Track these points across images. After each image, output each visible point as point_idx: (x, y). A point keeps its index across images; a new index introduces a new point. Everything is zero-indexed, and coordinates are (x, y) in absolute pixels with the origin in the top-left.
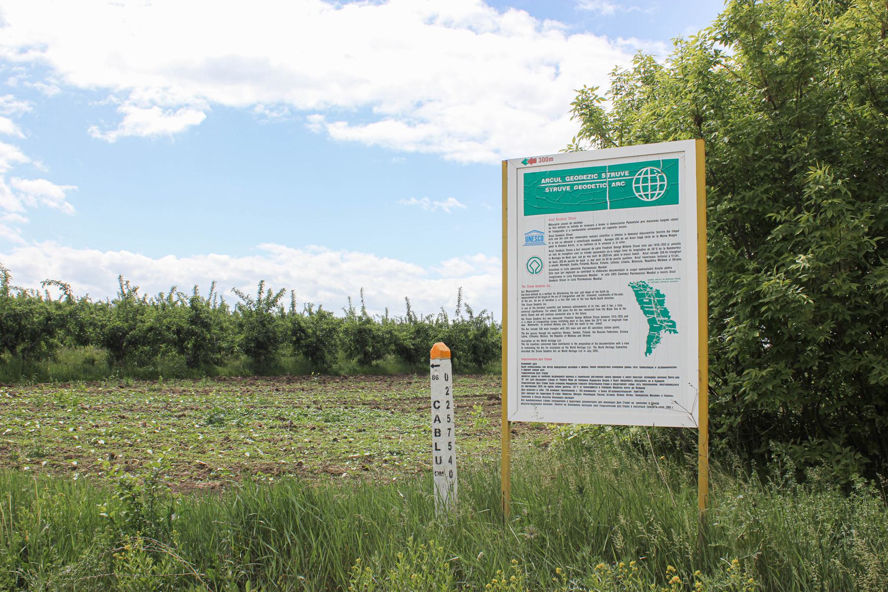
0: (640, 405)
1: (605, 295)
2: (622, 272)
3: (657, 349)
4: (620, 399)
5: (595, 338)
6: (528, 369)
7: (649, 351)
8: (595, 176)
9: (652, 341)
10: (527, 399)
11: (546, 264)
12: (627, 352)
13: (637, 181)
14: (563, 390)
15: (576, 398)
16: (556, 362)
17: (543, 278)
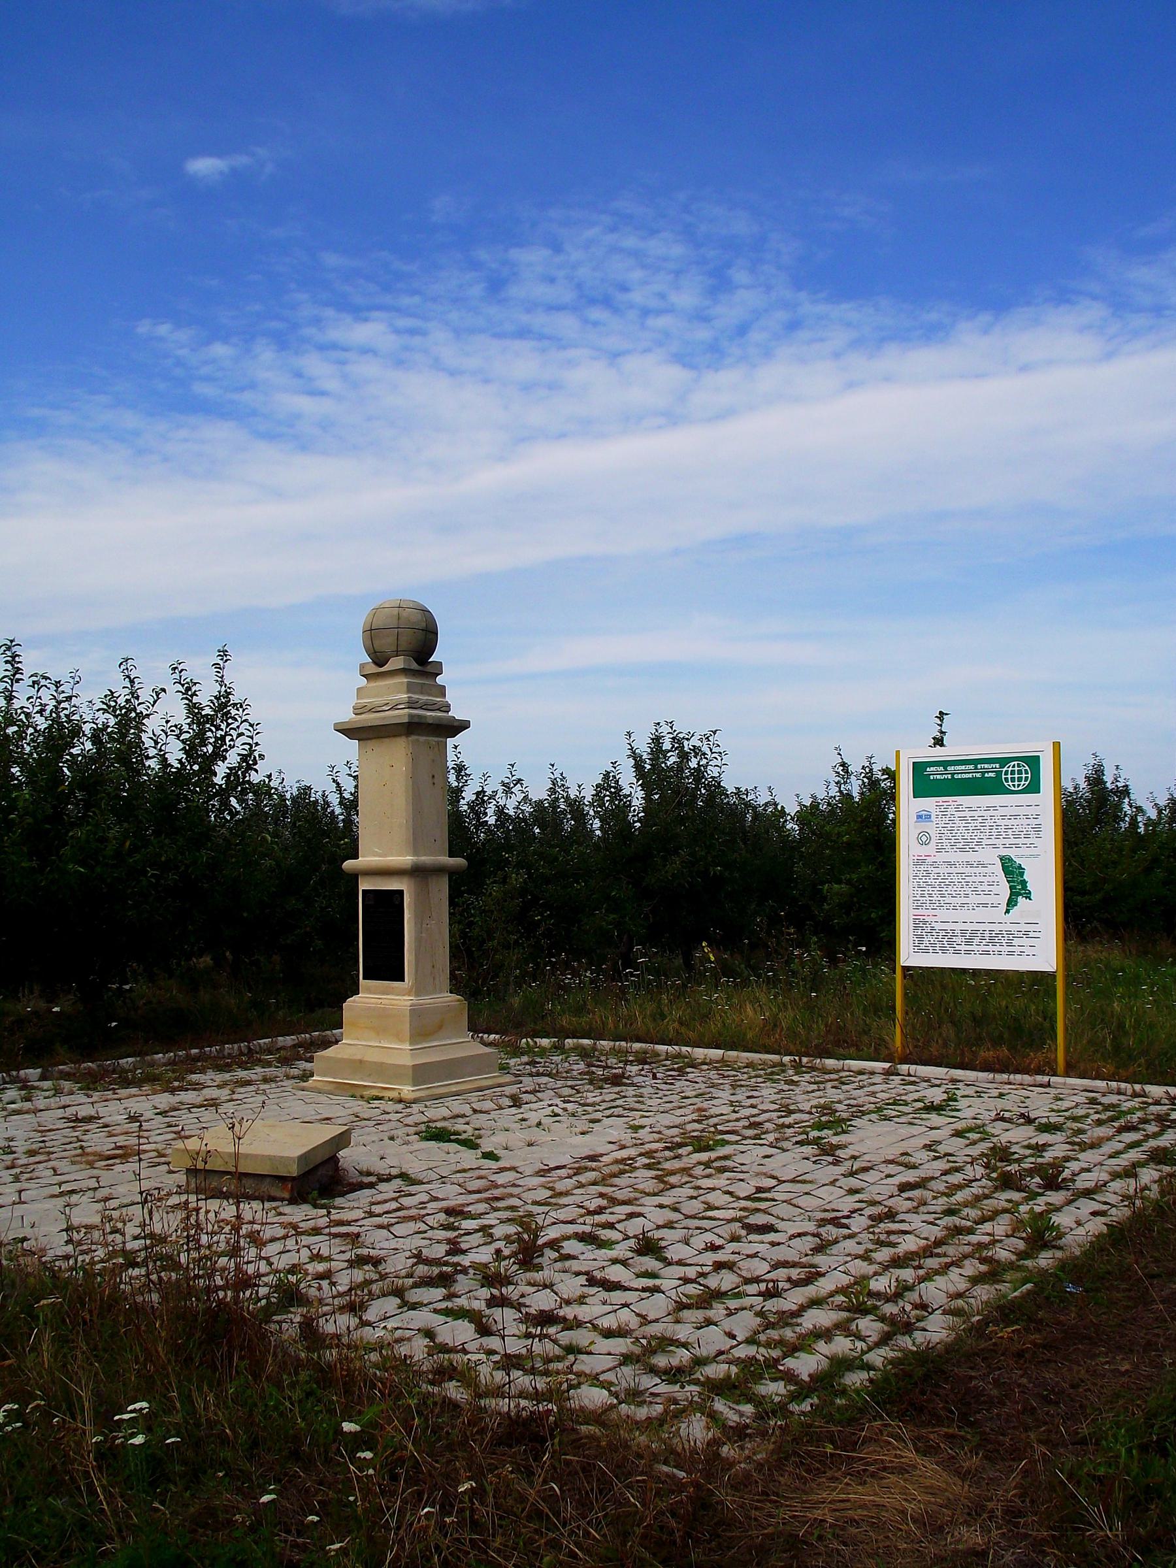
0: (1011, 953)
1: (981, 864)
4: (994, 948)
6: (918, 923)
7: (1007, 911)
8: (971, 767)
9: (1011, 903)
10: (919, 948)
13: (1006, 773)
17: (931, 849)
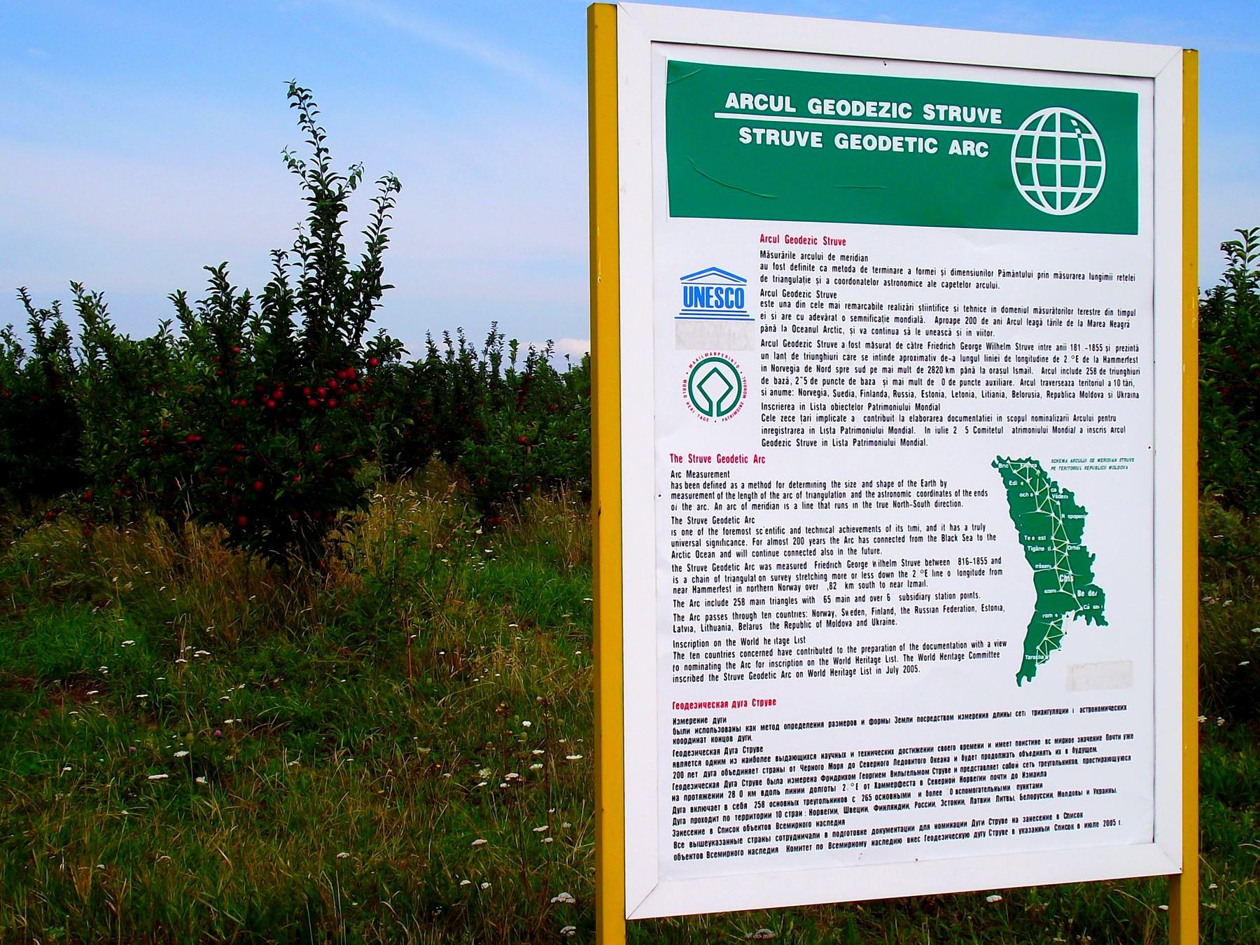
0: (1035, 824)
1: (935, 493)
2: (982, 426)
3: (1052, 667)
5: (912, 629)
6: (693, 733)
7: (1027, 670)
8: (902, 109)
9: (1041, 637)
10: (694, 842)
11: (751, 369)
12: (976, 695)
13: (1024, 149)
15: (853, 821)
16: (806, 711)
17: (742, 432)
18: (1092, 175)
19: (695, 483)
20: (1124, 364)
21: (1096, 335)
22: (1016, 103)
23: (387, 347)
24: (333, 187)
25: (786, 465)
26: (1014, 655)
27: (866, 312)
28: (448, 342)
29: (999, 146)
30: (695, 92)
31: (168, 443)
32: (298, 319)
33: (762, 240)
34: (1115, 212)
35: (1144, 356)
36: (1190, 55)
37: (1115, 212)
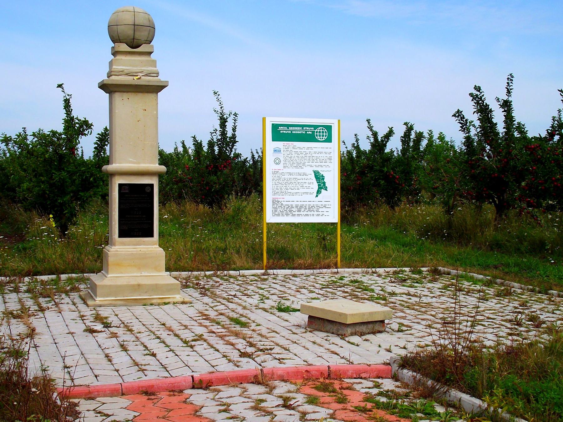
0: (318, 215)
1: (305, 174)
2: (311, 166)
3: (320, 196)
6: (274, 202)
7: (317, 196)
8: (301, 128)
9: (319, 192)
10: (275, 214)
11: (282, 159)
12: (310, 198)
13: (317, 132)
14: (289, 210)
15: (294, 213)
16: (287, 199)
17: (281, 166)
18: (326, 136)
19: (275, 172)
20: (330, 159)
21: (326, 155)
22: (316, 127)
23: (238, 156)
24: (225, 116)
25: (286, 170)
26: (315, 194)
27: (296, 152)
28: (257, 153)
29: (313, 132)
30: (275, 127)
31: (181, 180)
32: (216, 148)
33: (367, 120)
34: (329, 140)
35: (333, 158)
36: (339, 121)
37: (329, 140)
